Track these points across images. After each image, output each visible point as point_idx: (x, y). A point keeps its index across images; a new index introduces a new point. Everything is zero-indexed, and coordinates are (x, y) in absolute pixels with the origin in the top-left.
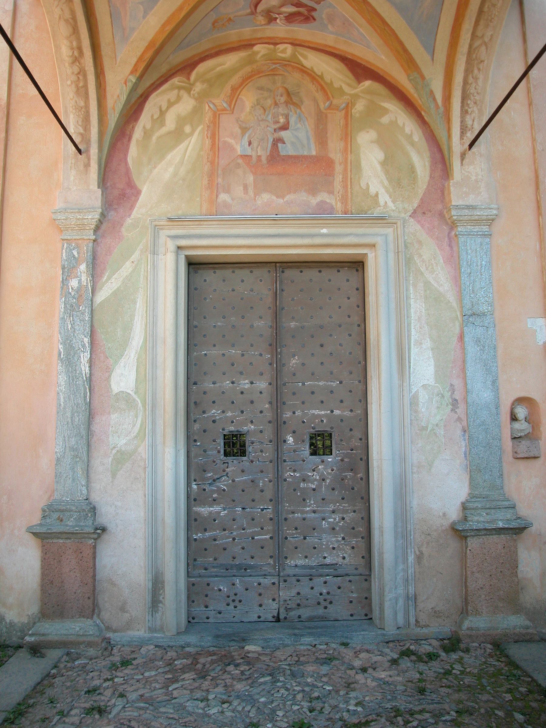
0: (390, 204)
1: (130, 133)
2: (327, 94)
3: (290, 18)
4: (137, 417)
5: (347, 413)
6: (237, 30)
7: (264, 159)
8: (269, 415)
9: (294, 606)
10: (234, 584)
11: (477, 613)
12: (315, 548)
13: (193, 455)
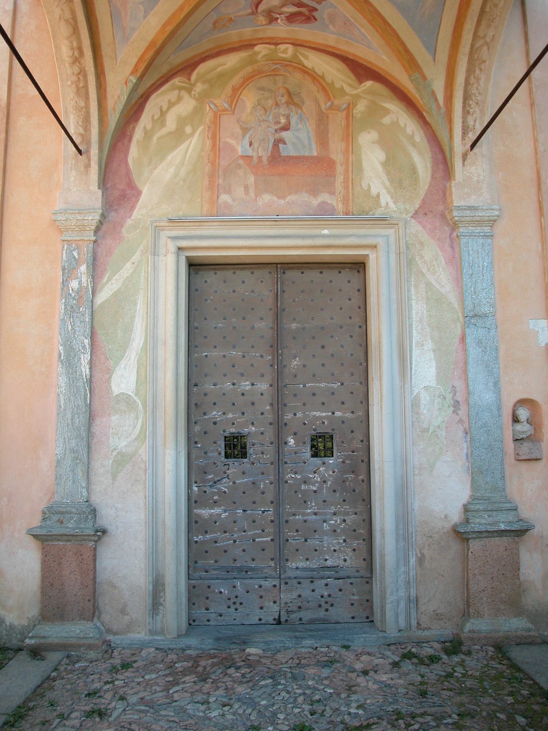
0: (392, 205)
1: (131, 133)
2: (328, 95)
3: (291, 18)
4: (137, 418)
5: (348, 415)
6: (238, 31)
7: (265, 159)
8: (270, 417)
9: (295, 608)
10: (234, 587)
11: (479, 615)
12: (316, 550)
13: (193, 456)
